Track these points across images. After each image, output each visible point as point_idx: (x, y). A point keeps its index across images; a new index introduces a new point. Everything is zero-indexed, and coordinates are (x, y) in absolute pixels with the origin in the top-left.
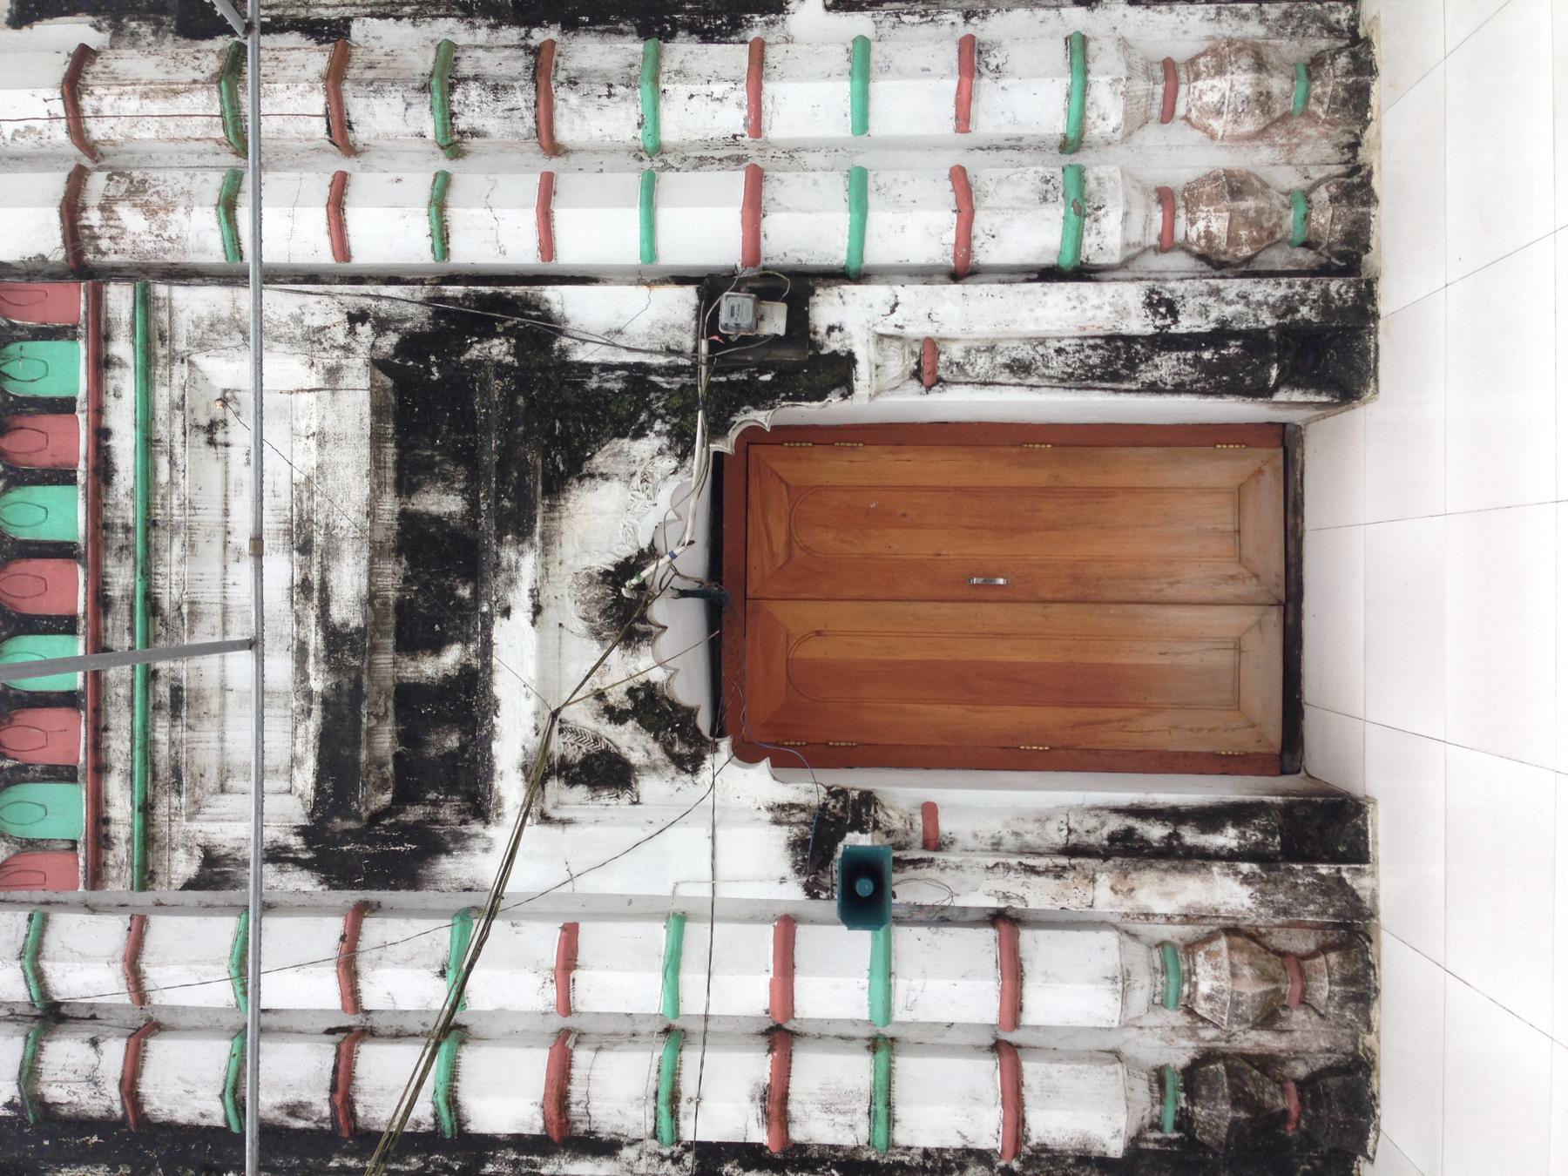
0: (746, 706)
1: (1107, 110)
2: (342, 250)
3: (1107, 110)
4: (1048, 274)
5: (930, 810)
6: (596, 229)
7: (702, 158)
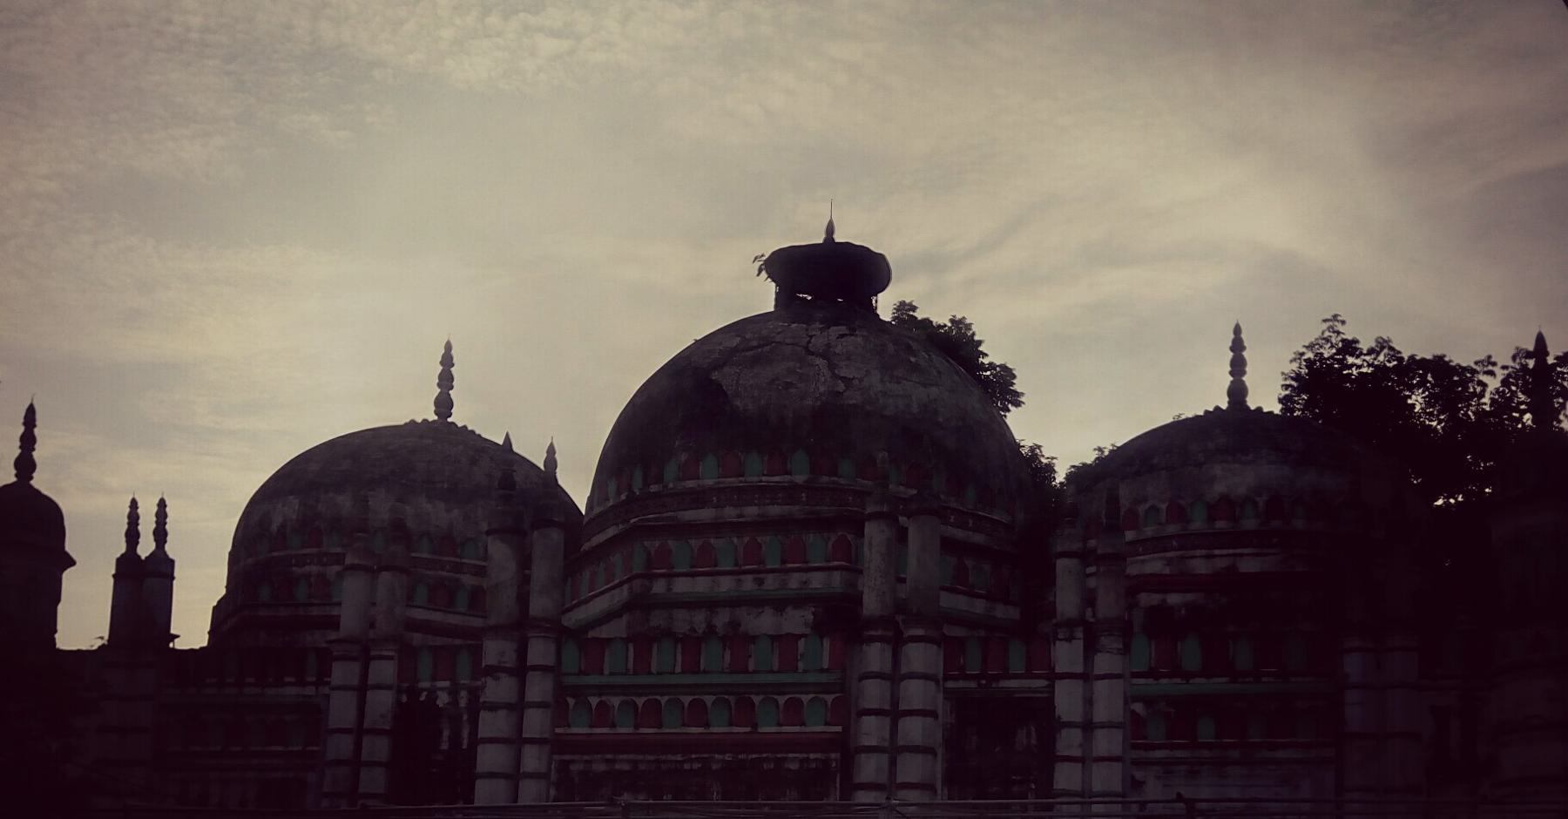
2: (509, 707)
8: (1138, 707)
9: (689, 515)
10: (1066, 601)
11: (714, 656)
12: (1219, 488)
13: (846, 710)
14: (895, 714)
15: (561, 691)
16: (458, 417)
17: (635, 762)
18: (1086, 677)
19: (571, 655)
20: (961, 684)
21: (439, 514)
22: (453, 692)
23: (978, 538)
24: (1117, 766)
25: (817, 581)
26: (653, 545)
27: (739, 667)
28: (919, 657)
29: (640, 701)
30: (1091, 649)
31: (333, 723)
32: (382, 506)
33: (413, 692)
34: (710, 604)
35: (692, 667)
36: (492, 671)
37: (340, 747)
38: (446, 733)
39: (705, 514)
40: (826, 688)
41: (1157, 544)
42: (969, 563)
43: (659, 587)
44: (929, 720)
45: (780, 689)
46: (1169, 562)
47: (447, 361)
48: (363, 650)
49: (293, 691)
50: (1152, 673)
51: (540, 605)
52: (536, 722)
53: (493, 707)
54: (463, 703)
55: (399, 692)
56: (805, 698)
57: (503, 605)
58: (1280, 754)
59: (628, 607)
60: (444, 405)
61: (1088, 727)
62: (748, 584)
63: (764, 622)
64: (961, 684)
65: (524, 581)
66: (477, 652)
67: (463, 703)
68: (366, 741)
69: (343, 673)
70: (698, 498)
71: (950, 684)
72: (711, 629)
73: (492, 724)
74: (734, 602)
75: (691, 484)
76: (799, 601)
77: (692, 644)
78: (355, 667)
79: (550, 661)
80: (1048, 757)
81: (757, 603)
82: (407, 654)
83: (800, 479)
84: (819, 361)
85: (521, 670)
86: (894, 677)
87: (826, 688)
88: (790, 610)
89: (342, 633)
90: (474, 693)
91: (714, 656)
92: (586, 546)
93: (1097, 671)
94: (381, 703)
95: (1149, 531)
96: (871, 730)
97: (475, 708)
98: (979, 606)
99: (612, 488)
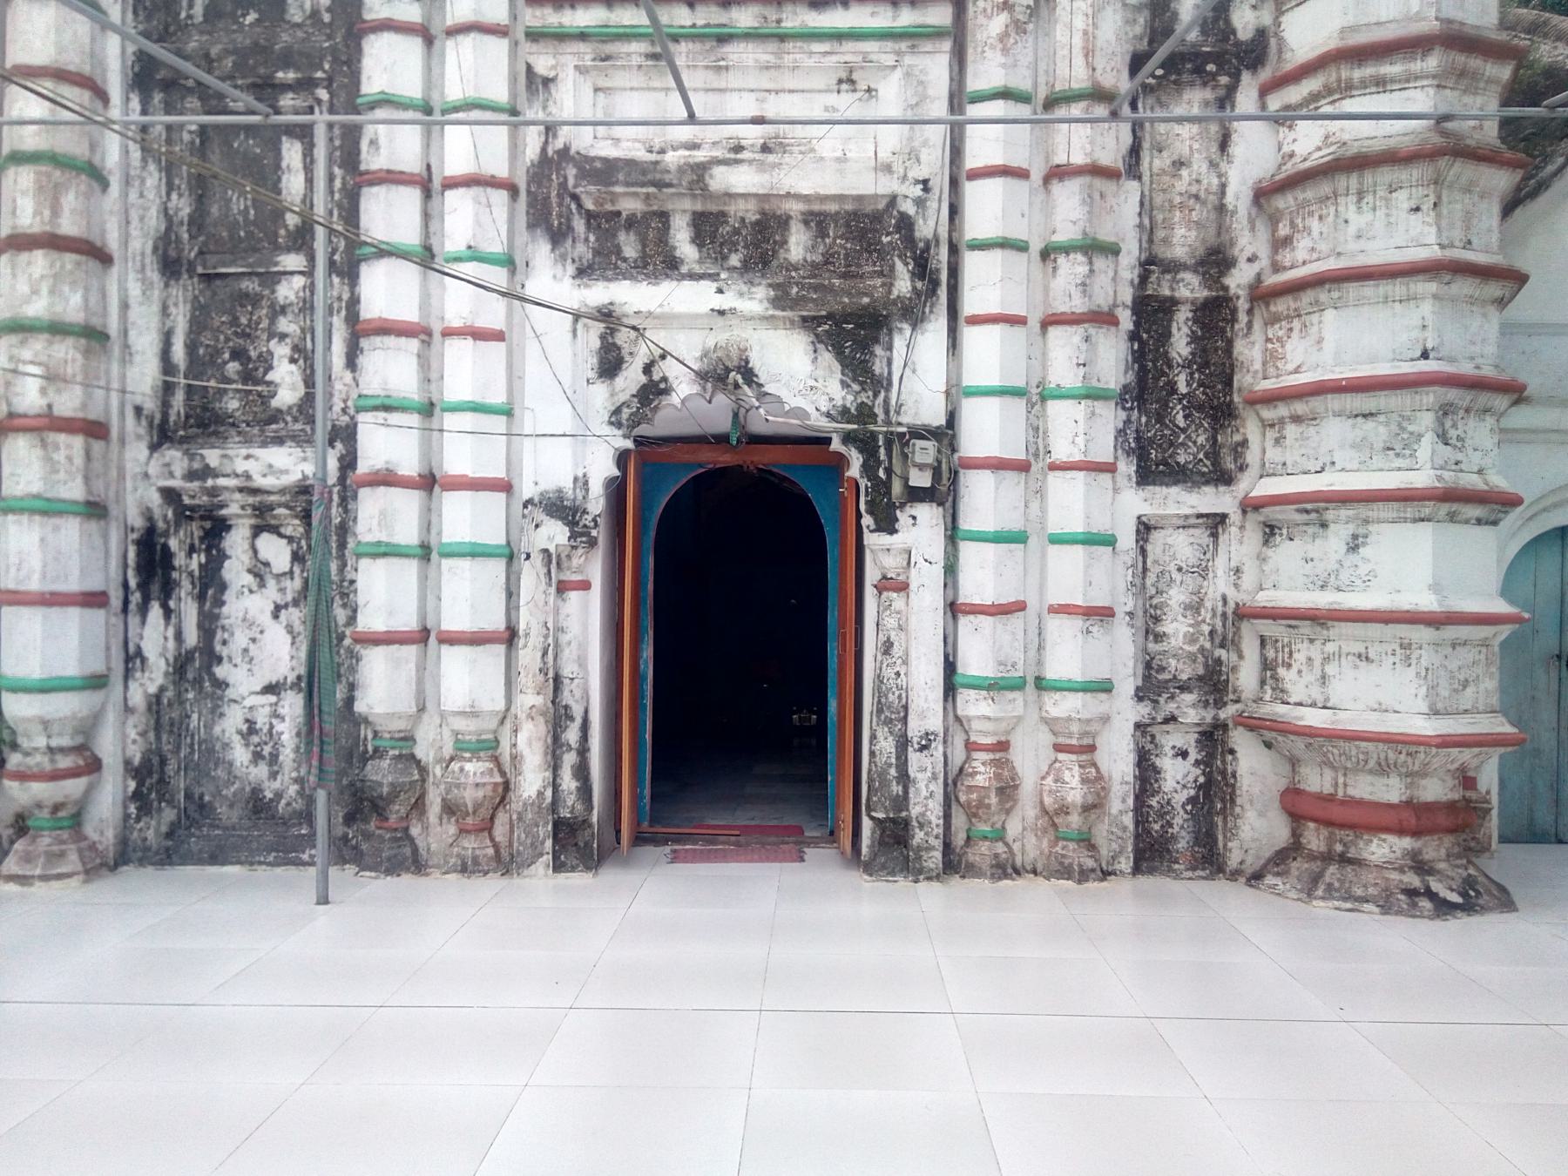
1: (1063, 706)
3: (1063, 706)
4: (950, 667)
6: (987, 356)
31: (371, 620)
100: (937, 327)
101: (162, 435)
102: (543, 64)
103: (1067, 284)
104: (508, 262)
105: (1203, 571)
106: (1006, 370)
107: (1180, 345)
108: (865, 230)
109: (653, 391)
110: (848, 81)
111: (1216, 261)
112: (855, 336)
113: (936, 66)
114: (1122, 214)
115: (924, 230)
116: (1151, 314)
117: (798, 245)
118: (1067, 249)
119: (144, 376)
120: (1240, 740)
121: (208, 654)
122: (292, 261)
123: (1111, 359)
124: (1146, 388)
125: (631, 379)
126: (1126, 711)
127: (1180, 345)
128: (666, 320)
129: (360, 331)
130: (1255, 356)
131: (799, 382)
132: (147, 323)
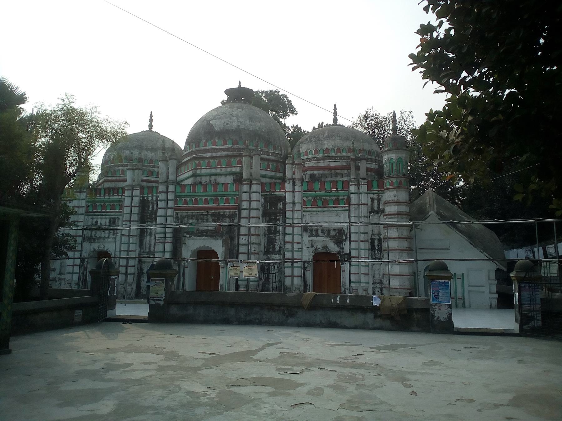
0: (318, 255)
1: (363, 285)
2: (164, 200)
3: (363, 285)
4: (350, 280)
5: (215, 180)
6: (353, 245)
7: (359, 253)
8: (305, 199)
9: (205, 155)
10: (289, 175)
11: (210, 189)
12: (326, 146)
13: (239, 200)
14: (250, 201)
15: (176, 197)
16: (154, 129)
17: (224, 212)
18: (293, 192)
19: (178, 189)
20: (265, 194)
21: (150, 155)
22: (152, 197)
23: (273, 158)
24: (300, 212)
25: (234, 170)
26: (197, 162)
27: (215, 191)
28: (255, 188)
29: (193, 199)
30: (294, 185)
31: (286, 274)
32: (136, 153)
33: (143, 197)
34: (210, 175)
35: (205, 191)
36: (160, 192)
37: (127, 210)
38: (151, 206)
39: (209, 155)
40: (235, 195)
41: (312, 159)
42: (270, 164)
43: (198, 172)
44: (258, 202)
45: (224, 195)
46: (315, 163)
47: (151, 116)
48: (132, 188)
49: (117, 197)
50: (308, 191)
51: (171, 177)
52: (171, 204)
53: (161, 201)
54: (154, 199)
55: (140, 197)
56: (230, 198)
57: (162, 178)
58: (336, 209)
59: (192, 176)
60: (151, 126)
61: (293, 203)
62: (218, 171)
63: (222, 180)
64: (265, 194)
65: (168, 173)
66: (157, 188)
67: (154, 199)
68: (133, 208)
69: (127, 193)
70: (207, 151)
71: (263, 194)
72: (210, 181)
73: (160, 204)
74: (215, 175)
75: (205, 148)
76: (230, 174)
77: (205, 186)
78: (130, 192)
79: (174, 190)
80: (284, 211)
81: (220, 175)
82: (142, 189)
83: (230, 146)
84: (235, 118)
85: (167, 192)
86: (250, 193)
87: (235, 195)
88: (228, 176)
89: (127, 184)
90: (157, 197)
91: (210, 189)
92: (183, 161)
93: (296, 190)
94: (136, 200)
95: (310, 156)
96: (245, 205)
97: (157, 201)
98: (273, 174)
99: (188, 147)
100: (348, 242)
101: (264, 254)
102: (305, 214)
103: (362, 237)
104: (301, 235)
105: (380, 269)
106: (356, 246)
107: (376, 244)
108: (340, 232)
109: (317, 249)
110: (337, 215)
111: (379, 235)
112: (339, 242)
113: (347, 214)
114: (368, 229)
115: (346, 232)
116: (373, 241)
117: (332, 233)
118: (362, 233)
119: (262, 248)
120: (384, 289)
121: (268, 278)
122: (278, 234)
123: (367, 245)
124: (373, 248)
125: (314, 248)
126: (371, 286)
127: (376, 244)
128: (318, 241)
129: (285, 243)
130: (384, 245)
131: (333, 247)
132: (263, 241)
